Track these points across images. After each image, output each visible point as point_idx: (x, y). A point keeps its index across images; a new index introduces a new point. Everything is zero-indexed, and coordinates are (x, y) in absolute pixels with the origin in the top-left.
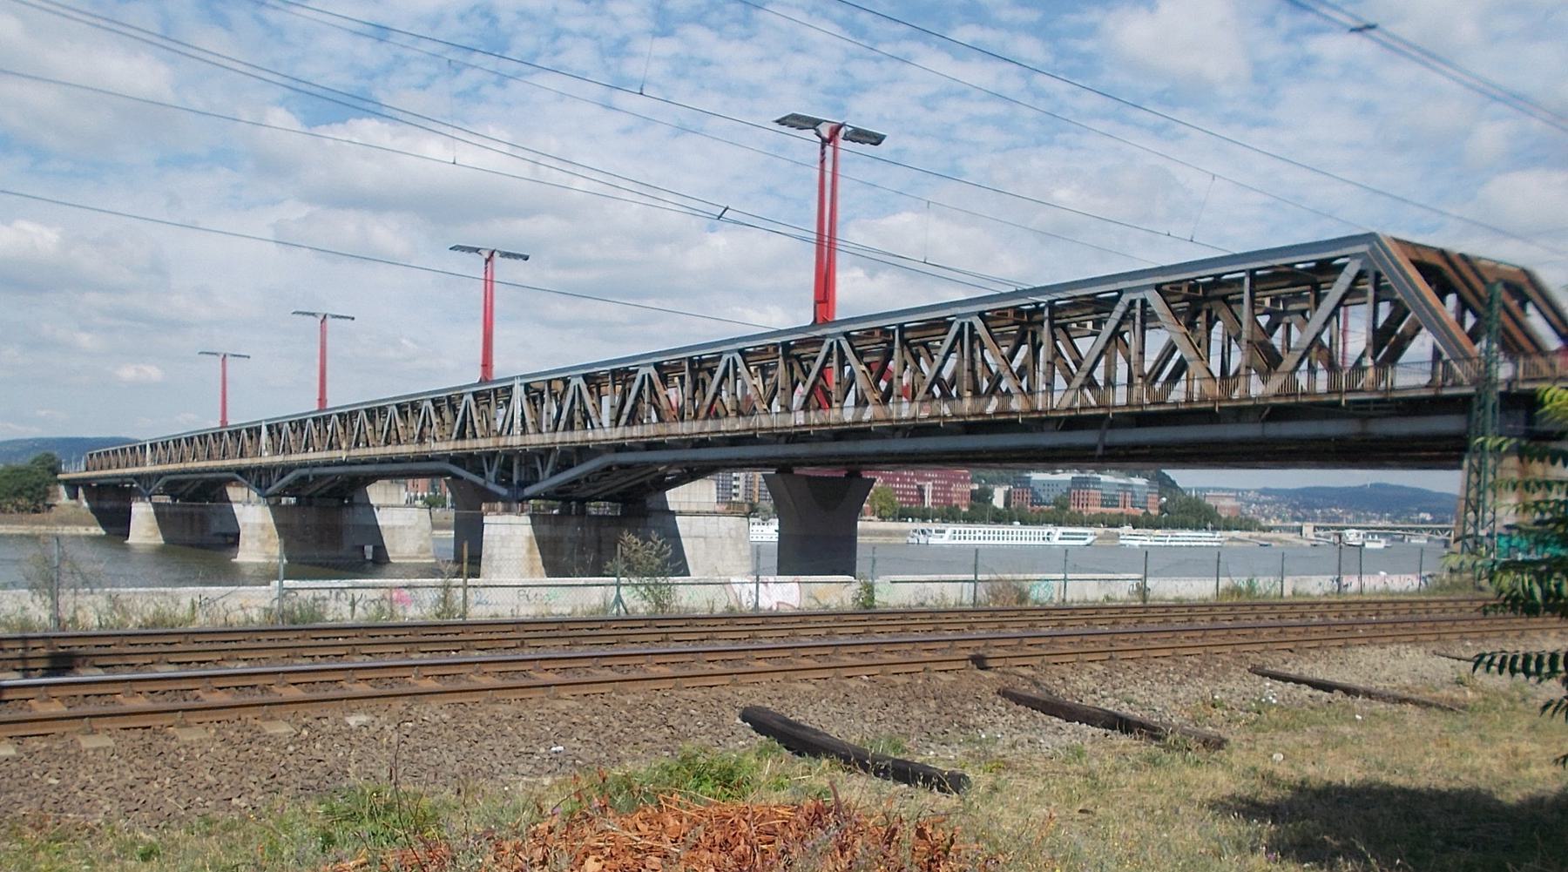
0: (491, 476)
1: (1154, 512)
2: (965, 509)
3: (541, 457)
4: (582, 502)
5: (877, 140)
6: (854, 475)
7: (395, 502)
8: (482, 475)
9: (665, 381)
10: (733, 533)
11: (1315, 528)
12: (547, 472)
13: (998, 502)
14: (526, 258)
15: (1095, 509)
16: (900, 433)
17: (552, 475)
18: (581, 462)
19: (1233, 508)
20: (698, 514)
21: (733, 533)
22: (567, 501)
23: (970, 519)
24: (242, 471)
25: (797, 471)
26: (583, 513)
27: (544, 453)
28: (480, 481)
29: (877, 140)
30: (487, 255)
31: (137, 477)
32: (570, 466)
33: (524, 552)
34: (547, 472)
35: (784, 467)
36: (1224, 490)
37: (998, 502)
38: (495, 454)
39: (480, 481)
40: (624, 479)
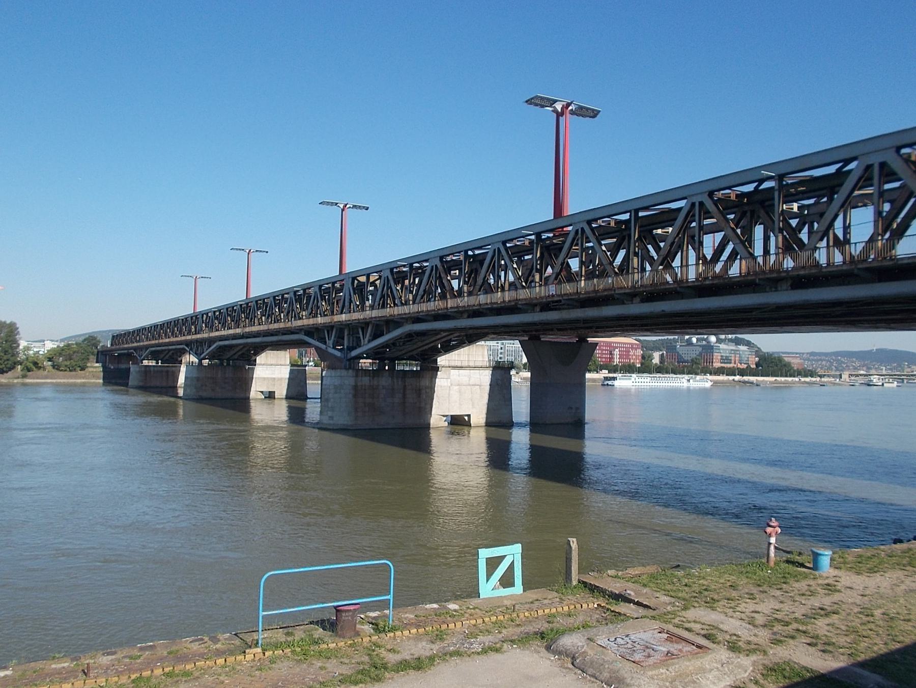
0: (330, 343)
1: (754, 366)
2: (639, 365)
3: (363, 329)
4: (392, 361)
5: (594, 114)
6: (582, 340)
7: (283, 363)
8: (325, 343)
9: (448, 271)
10: (500, 382)
11: (851, 375)
12: (366, 340)
13: (656, 360)
14: (367, 209)
15: (717, 365)
16: (638, 299)
17: (369, 341)
18: (389, 332)
19: (798, 363)
20: (461, 368)
21: (500, 382)
22: (382, 360)
23: (641, 371)
24: (188, 343)
25: (544, 338)
26: (392, 368)
27: (364, 325)
28: (323, 346)
29: (594, 114)
30: (342, 206)
31: (135, 349)
32: (382, 335)
33: (351, 396)
34: (366, 340)
35: (535, 338)
36: (793, 353)
37: (656, 360)
38: (332, 327)
39: (323, 346)
40: (420, 344)
